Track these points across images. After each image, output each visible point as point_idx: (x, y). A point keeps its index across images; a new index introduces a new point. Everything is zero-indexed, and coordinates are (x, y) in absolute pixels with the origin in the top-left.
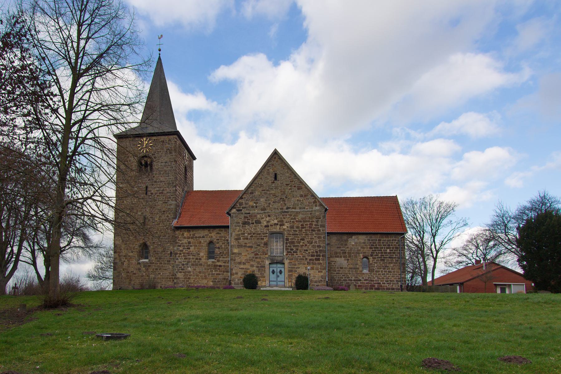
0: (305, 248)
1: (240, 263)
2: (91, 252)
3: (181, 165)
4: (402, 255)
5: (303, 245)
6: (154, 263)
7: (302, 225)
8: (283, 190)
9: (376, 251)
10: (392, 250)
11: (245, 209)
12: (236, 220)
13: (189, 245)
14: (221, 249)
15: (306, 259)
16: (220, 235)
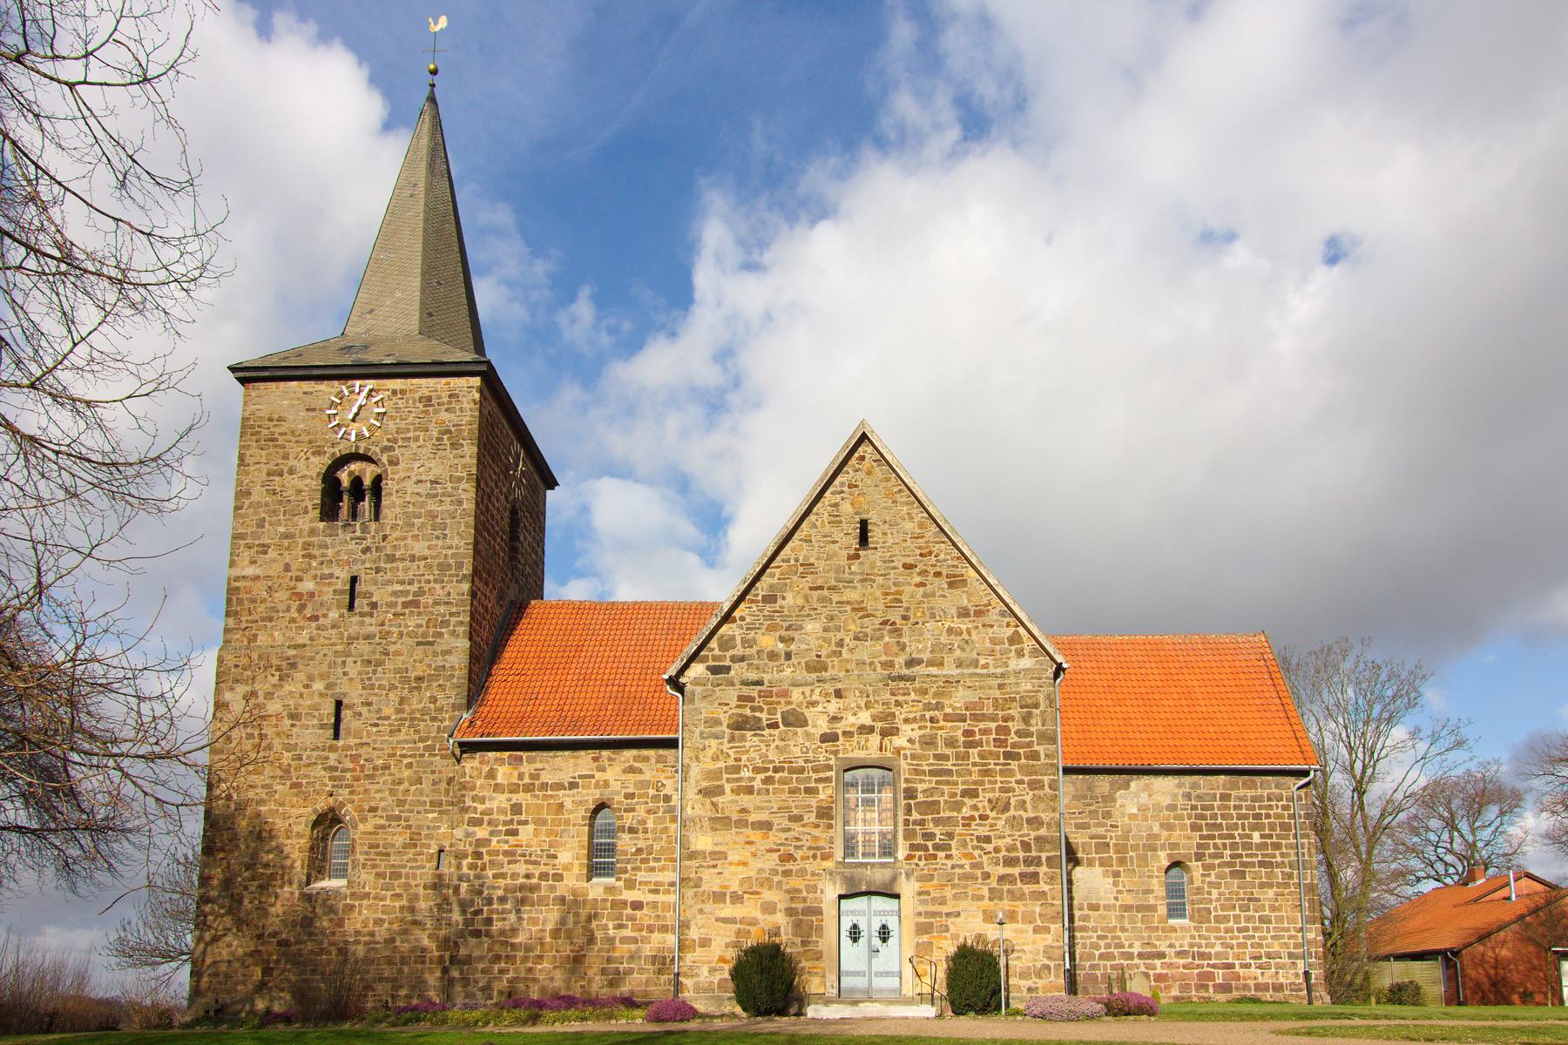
0: (983, 831)
1: (719, 897)
2: (74, 852)
3: (498, 499)
4: (1303, 854)
5: (972, 818)
6: (367, 895)
7: (968, 733)
8: (893, 589)
9: (1212, 837)
10: (1270, 836)
11: (744, 664)
12: (705, 709)
13: (516, 818)
14: (641, 835)
15: (987, 876)
16: (639, 777)
